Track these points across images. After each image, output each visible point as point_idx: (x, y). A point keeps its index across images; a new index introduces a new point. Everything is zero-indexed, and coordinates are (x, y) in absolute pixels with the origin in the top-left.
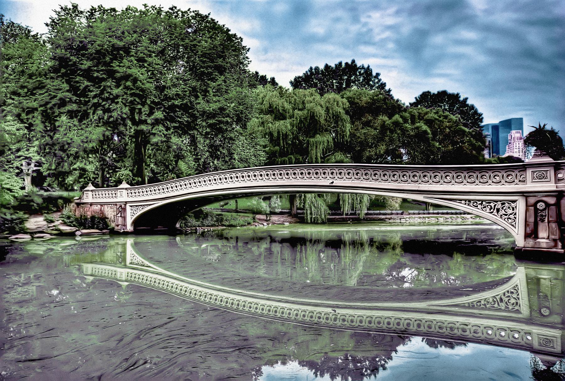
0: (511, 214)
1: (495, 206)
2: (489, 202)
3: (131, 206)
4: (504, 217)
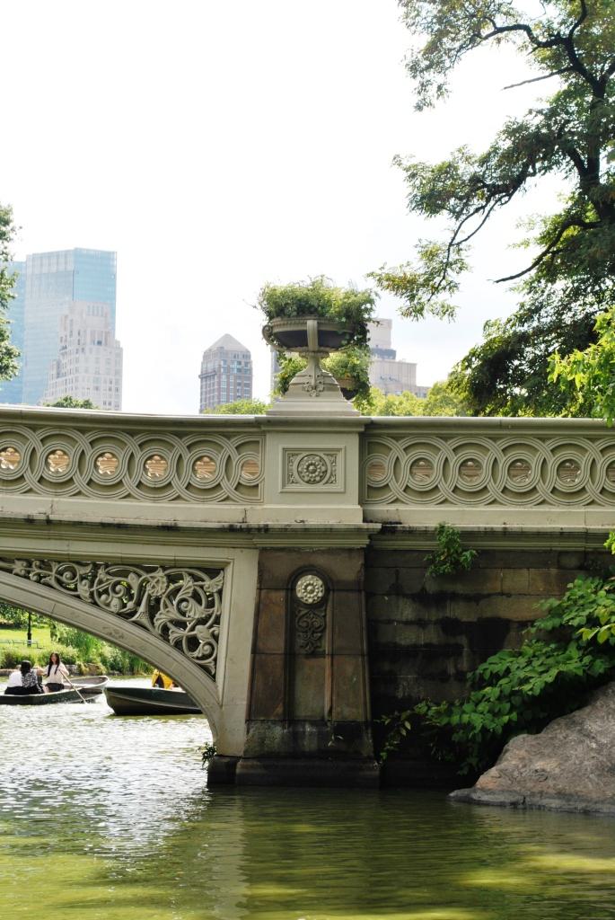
0: (202, 621)
2: (125, 567)
4: (175, 633)
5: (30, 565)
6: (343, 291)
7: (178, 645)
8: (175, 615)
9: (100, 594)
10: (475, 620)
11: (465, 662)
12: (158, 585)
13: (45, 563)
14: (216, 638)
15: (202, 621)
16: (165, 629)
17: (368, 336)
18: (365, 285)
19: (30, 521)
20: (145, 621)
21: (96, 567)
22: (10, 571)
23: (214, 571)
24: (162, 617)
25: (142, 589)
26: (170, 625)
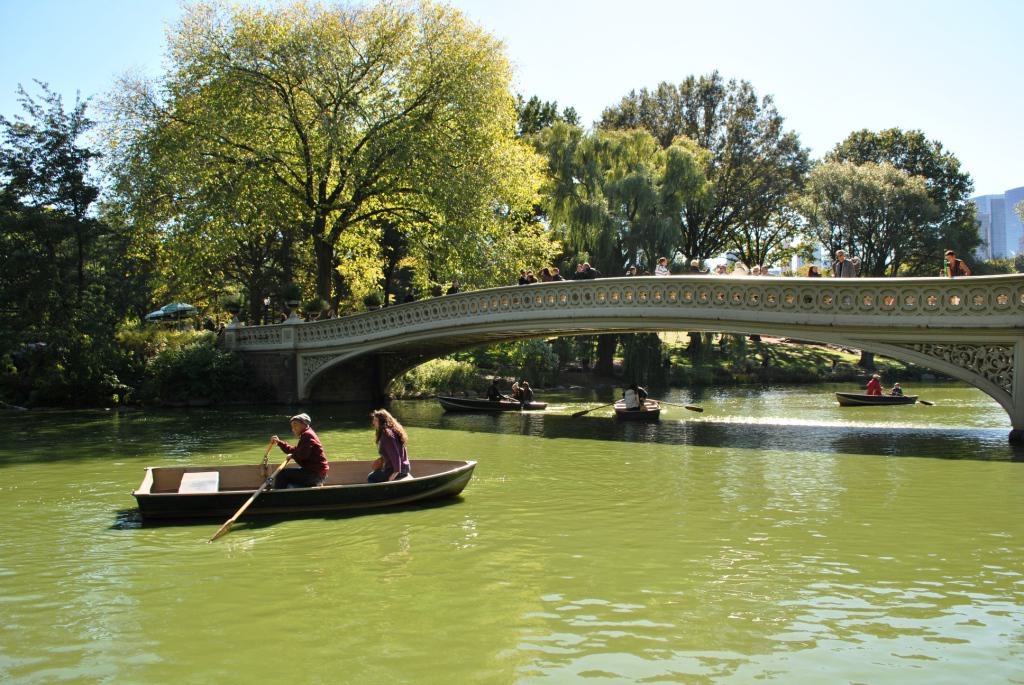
0: (1004, 370)
1: (975, 354)
2: (964, 347)
3: (305, 358)
4: (991, 375)
5: (921, 345)
6: (721, 83)
7: (992, 380)
8: (991, 367)
9: (954, 358)
10: (1007, 415)
11: (532, 615)
12: (982, 354)
13: (929, 346)
14: (1011, 377)
15: (1004, 370)
16: (986, 375)
17: (802, 147)
18: (931, 142)
19: (919, 327)
20: (976, 370)
21: (952, 346)
22: (913, 349)
23: (1012, 345)
24: (984, 368)
25: (975, 354)
26: (988, 372)
